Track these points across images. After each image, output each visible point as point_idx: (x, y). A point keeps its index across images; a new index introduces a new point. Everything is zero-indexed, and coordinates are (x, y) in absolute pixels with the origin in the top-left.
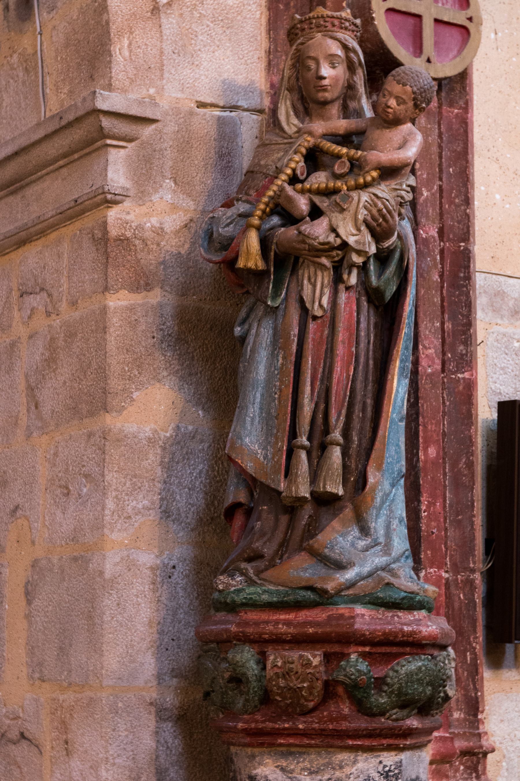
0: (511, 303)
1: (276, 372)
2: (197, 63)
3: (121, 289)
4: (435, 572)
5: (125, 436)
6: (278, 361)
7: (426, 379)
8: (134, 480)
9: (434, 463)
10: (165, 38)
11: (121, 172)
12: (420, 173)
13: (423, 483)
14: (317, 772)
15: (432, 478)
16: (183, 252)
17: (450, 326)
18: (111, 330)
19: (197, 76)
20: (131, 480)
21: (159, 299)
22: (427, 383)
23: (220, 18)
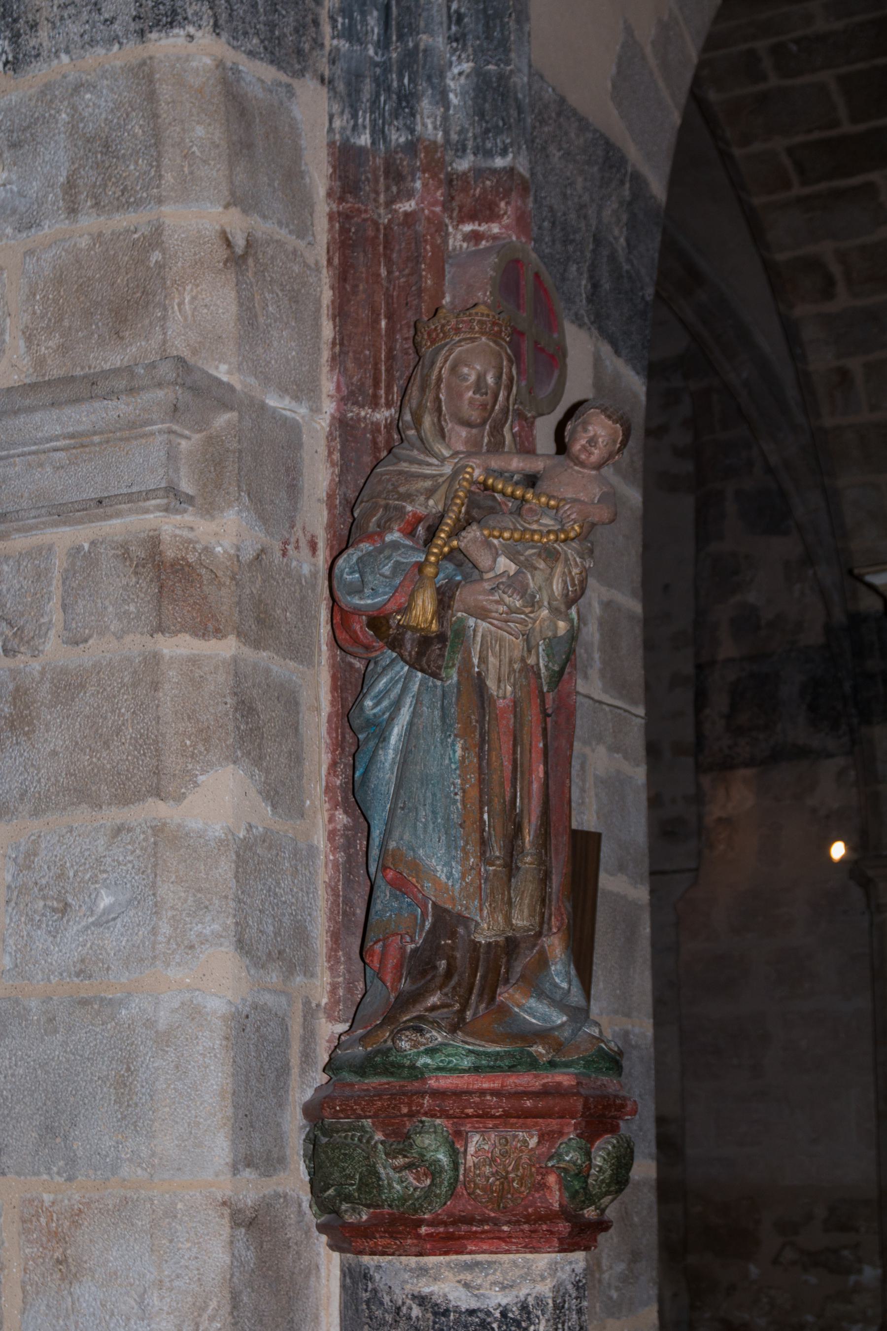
1: (453, 766)
3: (180, 632)
5: (187, 834)
6: (454, 752)
8: (199, 895)
14: (512, 1286)
18: (167, 686)
20: (195, 896)
21: (233, 651)
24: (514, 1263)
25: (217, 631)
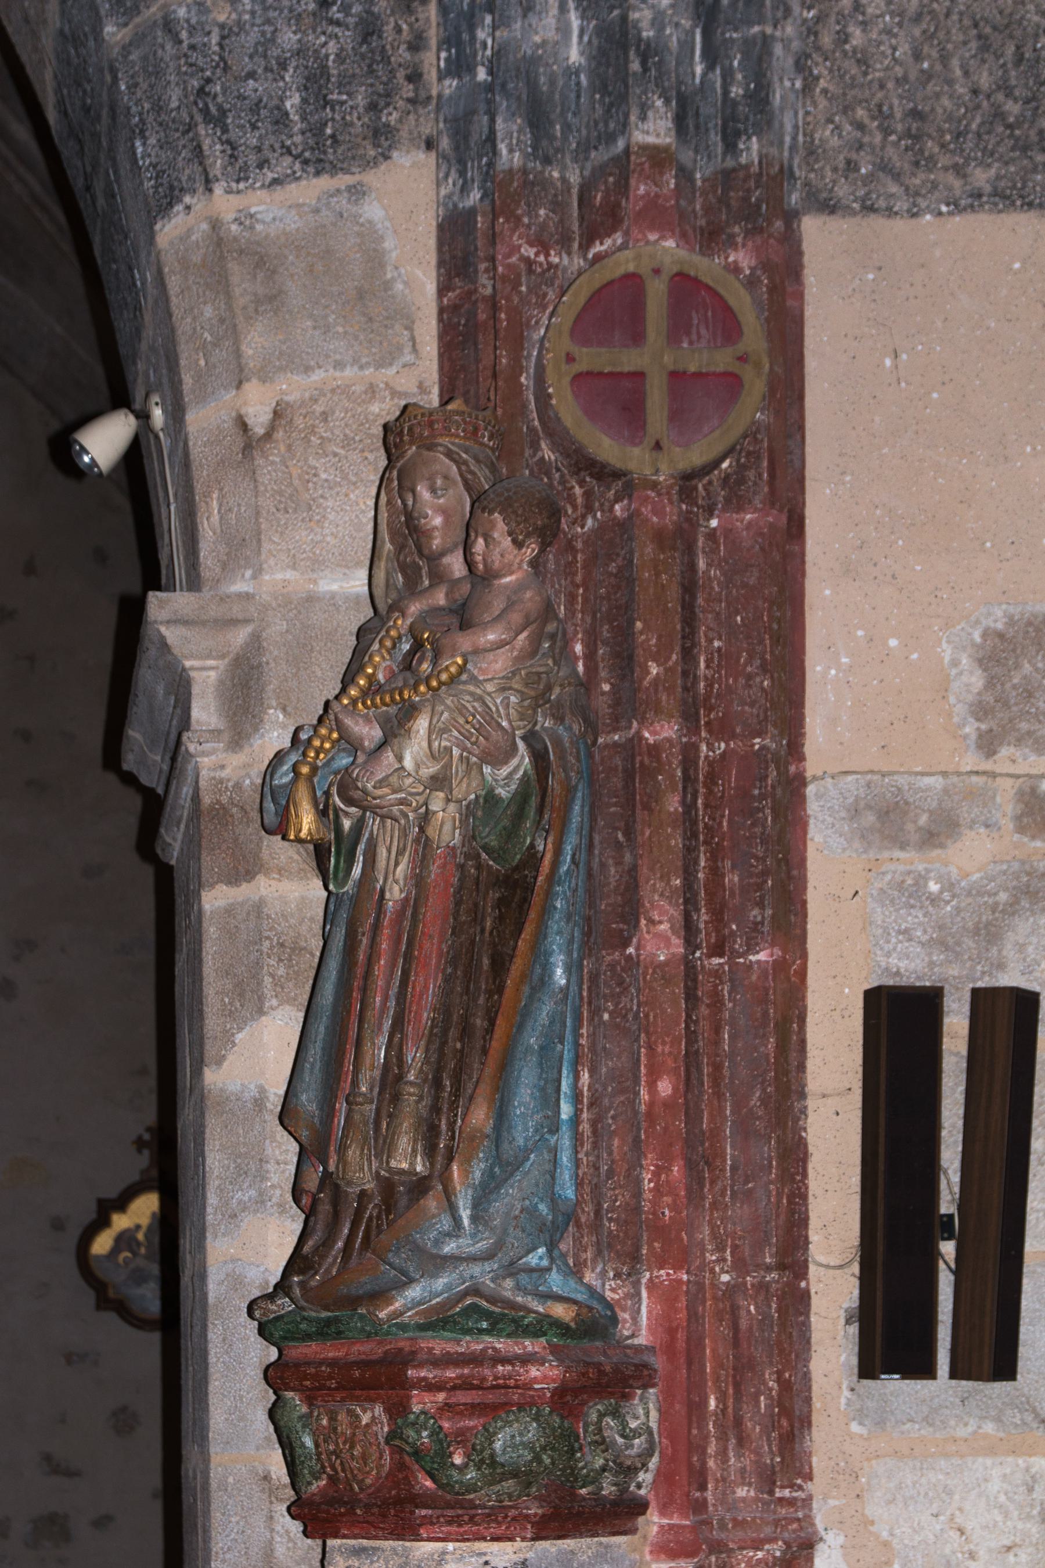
0: (923, 820)
2: (318, 517)
4: (668, 1274)
5: (227, 1099)
7: (654, 972)
9: (668, 1105)
10: (262, 488)
11: (212, 709)
12: (643, 637)
13: (647, 1137)
15: (666, 1129)
16: (502, 792)
17: (736, 879)
19: (319, 538)
22: (655, 980)
23: (357, 438)
24: (394, 1550)
25: (248, 872)
